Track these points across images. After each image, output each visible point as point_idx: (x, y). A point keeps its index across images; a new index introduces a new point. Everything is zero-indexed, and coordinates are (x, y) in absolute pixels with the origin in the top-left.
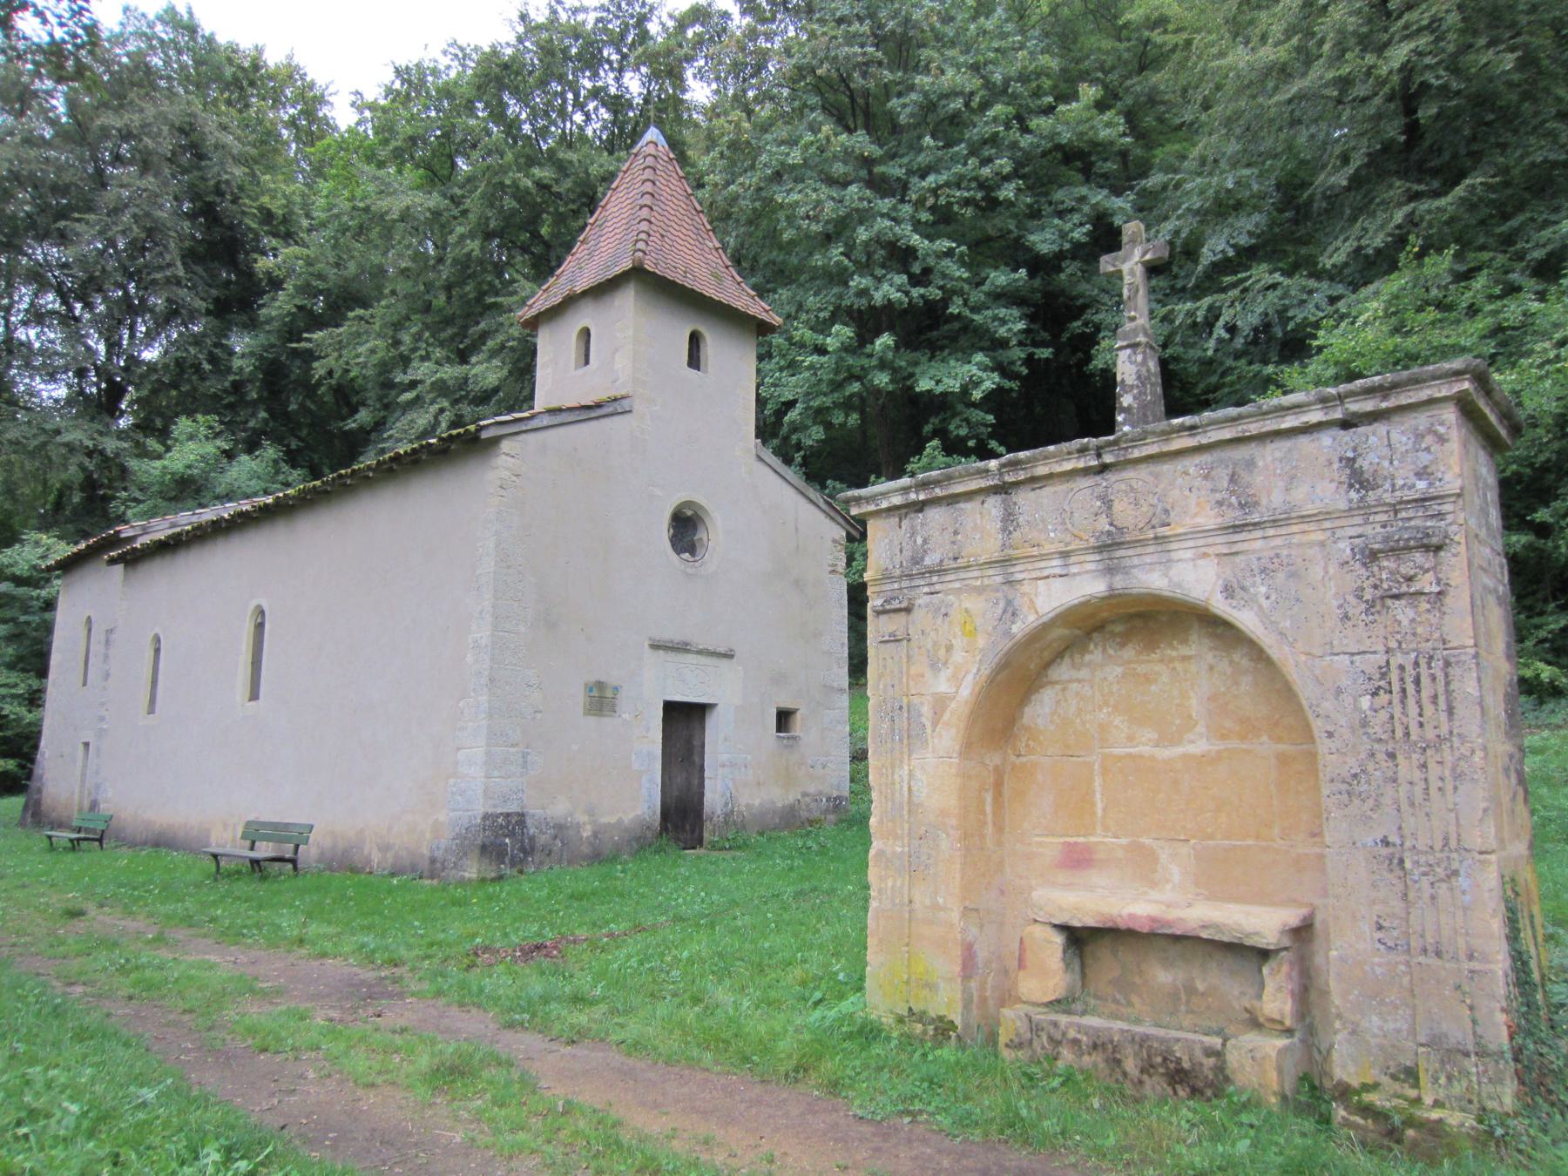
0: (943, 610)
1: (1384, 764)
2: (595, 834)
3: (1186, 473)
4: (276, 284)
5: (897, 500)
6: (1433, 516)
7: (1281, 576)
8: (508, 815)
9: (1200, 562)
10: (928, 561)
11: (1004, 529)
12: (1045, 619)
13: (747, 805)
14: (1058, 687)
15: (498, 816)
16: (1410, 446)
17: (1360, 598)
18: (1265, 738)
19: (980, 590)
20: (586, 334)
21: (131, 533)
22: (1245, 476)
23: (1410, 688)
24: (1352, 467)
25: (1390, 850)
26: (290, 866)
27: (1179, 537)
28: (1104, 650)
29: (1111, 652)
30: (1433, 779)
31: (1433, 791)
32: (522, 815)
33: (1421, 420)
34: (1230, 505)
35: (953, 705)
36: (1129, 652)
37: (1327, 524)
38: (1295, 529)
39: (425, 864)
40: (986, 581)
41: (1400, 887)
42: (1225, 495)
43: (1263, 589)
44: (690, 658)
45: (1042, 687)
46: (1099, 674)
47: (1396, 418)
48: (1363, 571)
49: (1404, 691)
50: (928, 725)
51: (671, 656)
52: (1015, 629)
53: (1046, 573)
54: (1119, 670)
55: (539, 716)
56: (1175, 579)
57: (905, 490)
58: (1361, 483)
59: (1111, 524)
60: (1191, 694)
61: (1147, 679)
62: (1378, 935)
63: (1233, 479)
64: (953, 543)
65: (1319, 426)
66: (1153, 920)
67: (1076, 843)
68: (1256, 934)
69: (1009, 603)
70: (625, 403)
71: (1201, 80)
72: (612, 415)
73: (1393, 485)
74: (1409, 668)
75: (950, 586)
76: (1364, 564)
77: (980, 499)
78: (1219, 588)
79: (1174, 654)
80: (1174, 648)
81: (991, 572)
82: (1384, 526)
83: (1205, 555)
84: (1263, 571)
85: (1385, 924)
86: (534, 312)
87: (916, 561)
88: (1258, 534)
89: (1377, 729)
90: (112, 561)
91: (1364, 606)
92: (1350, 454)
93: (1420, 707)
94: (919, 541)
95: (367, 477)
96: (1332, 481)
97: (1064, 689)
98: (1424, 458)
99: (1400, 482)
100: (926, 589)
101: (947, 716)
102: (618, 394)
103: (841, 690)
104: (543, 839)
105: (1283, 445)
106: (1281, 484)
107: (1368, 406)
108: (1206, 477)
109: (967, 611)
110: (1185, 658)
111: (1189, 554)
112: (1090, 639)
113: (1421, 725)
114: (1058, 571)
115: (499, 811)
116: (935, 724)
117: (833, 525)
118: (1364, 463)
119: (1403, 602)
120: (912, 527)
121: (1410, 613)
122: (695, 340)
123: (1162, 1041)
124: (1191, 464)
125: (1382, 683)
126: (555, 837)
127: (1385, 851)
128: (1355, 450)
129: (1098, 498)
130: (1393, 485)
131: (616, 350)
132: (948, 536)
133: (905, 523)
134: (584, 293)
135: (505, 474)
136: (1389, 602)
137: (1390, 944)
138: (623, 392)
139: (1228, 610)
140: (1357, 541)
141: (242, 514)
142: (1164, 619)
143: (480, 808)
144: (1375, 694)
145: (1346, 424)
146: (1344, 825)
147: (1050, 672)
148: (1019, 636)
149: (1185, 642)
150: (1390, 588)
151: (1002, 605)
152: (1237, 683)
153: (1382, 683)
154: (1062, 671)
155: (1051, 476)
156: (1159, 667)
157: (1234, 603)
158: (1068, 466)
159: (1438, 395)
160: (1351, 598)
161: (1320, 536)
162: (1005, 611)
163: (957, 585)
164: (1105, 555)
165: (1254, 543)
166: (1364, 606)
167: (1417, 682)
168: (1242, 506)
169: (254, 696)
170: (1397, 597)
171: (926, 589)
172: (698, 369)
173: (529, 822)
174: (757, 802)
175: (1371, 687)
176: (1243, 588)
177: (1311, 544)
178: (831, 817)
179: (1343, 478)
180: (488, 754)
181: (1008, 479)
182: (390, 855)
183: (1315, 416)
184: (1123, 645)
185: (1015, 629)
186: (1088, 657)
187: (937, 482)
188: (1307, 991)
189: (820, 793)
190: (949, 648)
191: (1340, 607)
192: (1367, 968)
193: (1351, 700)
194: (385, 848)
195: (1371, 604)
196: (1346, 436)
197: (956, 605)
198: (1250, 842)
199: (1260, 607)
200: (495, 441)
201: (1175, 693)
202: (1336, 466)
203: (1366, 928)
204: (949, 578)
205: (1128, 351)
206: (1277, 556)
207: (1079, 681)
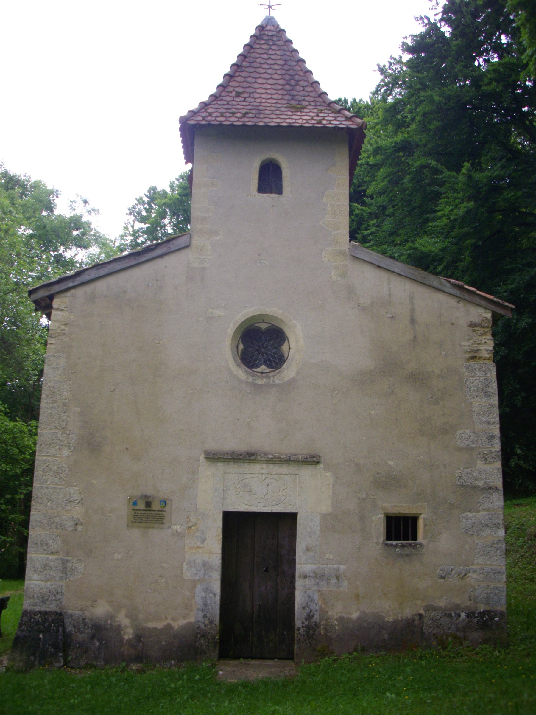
2: (138, 637)
4: (410, 128)
8: (46, 613)
13: (341, 619)
15: (36, 613)
44: (258, 468)
51: (233, 469)
71: (24, 325)
72: (166, 254)
103: (490, 489)
115: (37, 609)
117: (441, 297)
126: (93, 637)
173: (67, 621)
174: (355, 615)
178: (476, 635)
188: (257, 114)
189: (457, 607)
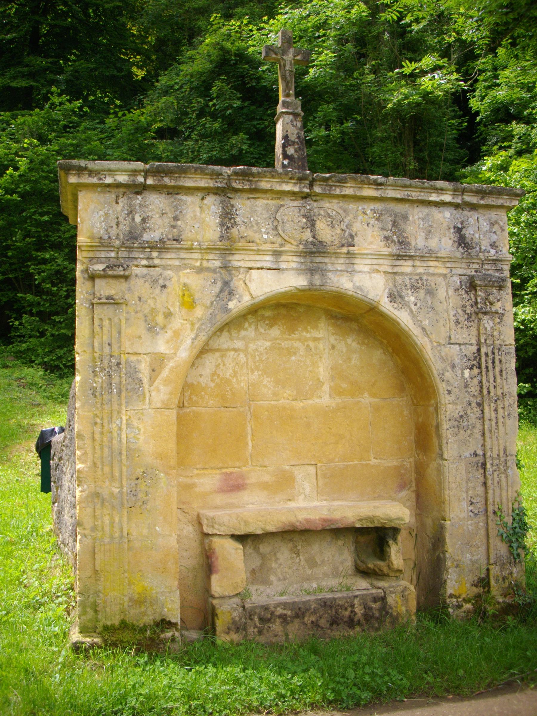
0: (161, 282)
1: (475, 409)
3: (365, 213)
5: (122, 178)
6: (498, 270)
7: (422, 293)
9: (374, 275)
10: (146, 237)
11: (222, 224)
12: (257, 300)
14: (217, 354)
16: (488, 228)
17: (465, 311)
18: (366, 395)
19: (200, 270)
22: (402, 225)
23: (490, 366)
24: (460, 233)
25: (477, 458)
27: (363, 256)
28: (256, 329)
29: (262, 330)
30: (500, 417)
31: (500, 424)
33: (493, 215)
34: (393, 241)
35: (172, 364)
36: (275, 332)
37: (448, 265)
38: (432, 264)
40: (205, 264)
41: (482, 479)
42: (389, 233)
43: (412, 299)
46: (252, 346)
47: (481, 211)
48: (465, 296)
49: (487, 367)
50: (145, 381)
52: (231, 305)
53: (259, 265)
56: (357, 284)
57: (135, 172)
58: (465, 244)
59: (314, 237)
60: (320, 364)
61: (291, 352)
62: (471, 508)
64: (173, 227)
65: (449, 204)
67: (231, 473)
68: (398, 519)
69: (226, 284)
73: (480, 249)
74: (490, 354)
75: (170, 262)
76: (467, 292)
77: (200, 195)
78: (386, 295)
79: (308, 335)
80: (307, 332)
81: (211, 256)
82: (476, 271)
83: (378, 271)
84: (413, 287)
85: (474, 501)
88: (410, 263)
89: (473, 389)
91: (466, 316)
92: (460, 226)
93: (495, 378)
94: (138, 219)
96: (450, 239)
98: (494, 237)
100: (145, 262)
101: (165, 373)
105: (426, 210)
106: (423, 234)
107: (474, 199)
108: (378, 219)
109: (185, 285)
110: (316, 339)
111: (366, 269)
112: (246, 319)
113: (495, 387)
114: (269, 265)
116: (152, 380)
118: (468, 232)
119: (488, 317)
121: (491, 323)
123: (304, 602)
124: (369, 207)
125: (475, 362)
127: (475, 459)
128: (462, 224)
129: (304, 216)
130: (480, 249)
132: (167, 220)
133: (122, 201)
136: (480, 315)
137: (476, 512)
139: (392, 309)
140: (463, 277)
142: (301, 310)
144: (471, 369)
146: (456, 446)
148: (234, 311)
149: (316, 327)
150: (482, 308)
151: (219, 284)
152: (350, 359)
153: (475, 362)
155: (271, 191)
156: (297, 344)
157: (396, 305)
158: (287, 187)
160: (460, 311)
161: (444, 271)
162: (221, 291)
163: (177, 263)
164: (308, 259)
165: (406, 267)
166: (466, 316)
167: (493, 362)
168: (400, 243)
170: (485, 313)
171: (145, 262)
175: (469, 364)
176: (401, 296)
177: (440, 275)
179: (456, 239)
184: (271, 326)
185: (231, 305)
186: (243, 333)
187: (169, 173)
191: (455, 315)
192: (465, 528)
193: (460, 372)
195: (470, 316)
196: (458, 214)
197: (175, 279)
198: (356, 462)
199: (411, 311)
201: (308, 362)
202: (452, 230)
203: (465, 504)
204: (169, 256)
205: (291, 117)
206: (421, 279)
207: (235, 350)
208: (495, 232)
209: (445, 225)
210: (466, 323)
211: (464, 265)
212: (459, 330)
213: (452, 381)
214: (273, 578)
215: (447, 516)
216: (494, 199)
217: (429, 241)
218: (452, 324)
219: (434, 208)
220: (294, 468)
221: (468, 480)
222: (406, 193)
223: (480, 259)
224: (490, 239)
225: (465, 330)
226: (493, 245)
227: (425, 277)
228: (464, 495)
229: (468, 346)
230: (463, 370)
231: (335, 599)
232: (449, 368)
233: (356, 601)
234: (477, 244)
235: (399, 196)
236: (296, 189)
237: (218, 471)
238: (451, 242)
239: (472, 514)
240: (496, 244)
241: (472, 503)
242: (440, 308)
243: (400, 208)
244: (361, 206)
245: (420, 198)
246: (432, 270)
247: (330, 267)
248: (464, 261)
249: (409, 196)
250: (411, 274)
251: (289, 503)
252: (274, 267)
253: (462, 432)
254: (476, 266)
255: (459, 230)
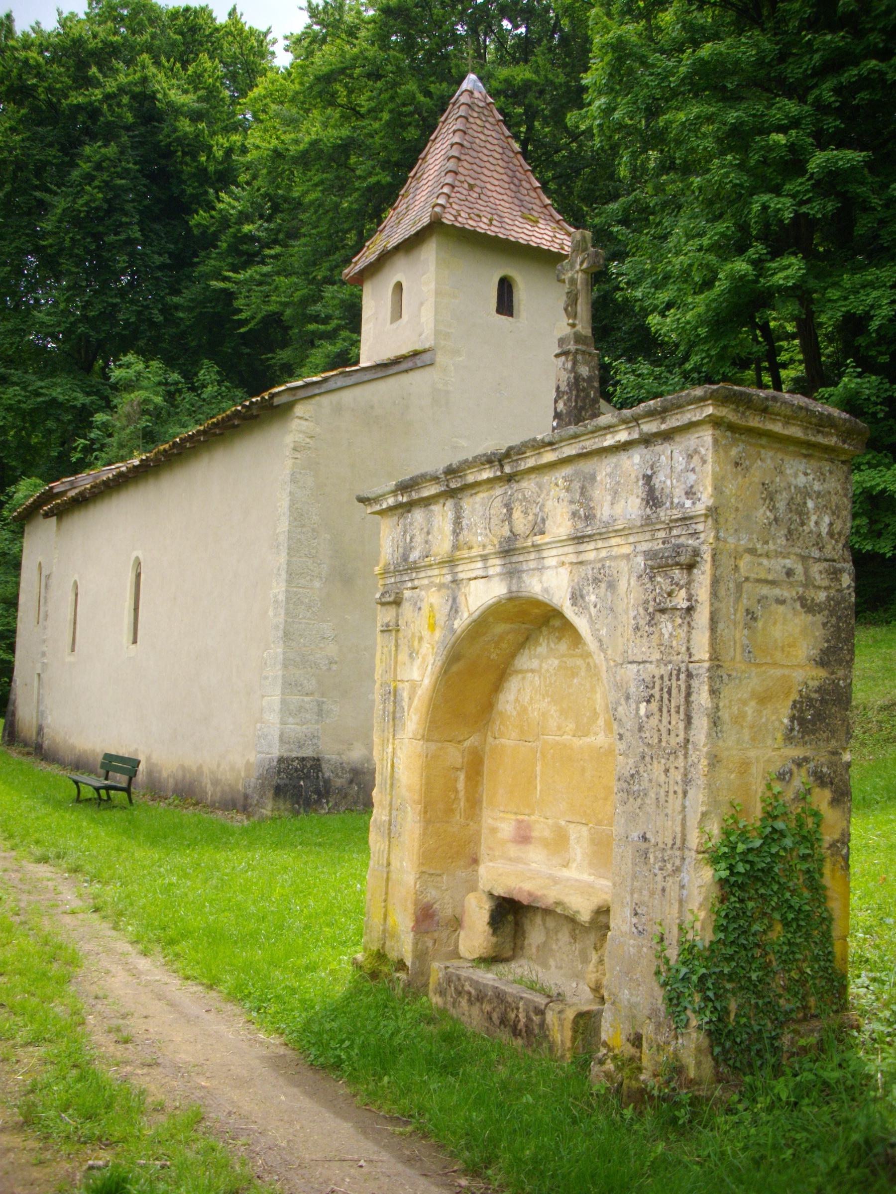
8: (303, 759)
14: (520, 676)
20: (399, 286)
21: (61, 489)
26: (124, 795)
29: (552, 645)
32: (318, 760)
37: (631, 539)
38: (614, 541)
39: (241, 801)
43: (593, 598)
45: (510, 675)
49: (662, 698)
53: (473, 575)
54: (556, 662)
55: (334, 667)
60: (598, 690)
62: (634, 920)
63: (583, 488)
65: (625, 446)
66: (530, 894)
70: (426, 357)
73: (672, 503)
78: (569, 596)
83: (563, 564)
85: (639, 911)
86: (357, 269)
87: (405, 558)
88: (592, 546)
90: (47, 515)
92: (649, 472)
95: (215, 435)
97: (524, 678)
99: (676, 500)
100: (409, 585)
102: (418, 347)
104: (338, 782)
114: (480, 573)
115: (294, 755)
118: (661, 479)
119: (666, 616)
120: (405, 526)
122: (505, 289)
124: (560, 475)
130: (672, 503)
131: (422, 304)
134: (397, 248)
135: (299, 437)
137: (640, 928)
138: (427, 346)
141: (121, 475)
143: (276, 752)
144: (648, 702)
145: (647, 440)
146: (623, 821)
147: (516, 662)
154: (524, 661)
159: (694, 419)
160: (641, 610)
161: (626, 550)
169: (135, 641)
171: (409, 585)
172: (511, 314)
179: (644, 496)
180: (283, 702)
181: (453, 485)
182: (219, 789)
183: (623, 436)
184: (560, 639)
186: (539, 649)
190: (421, 639)
191: (635, 618)
194: (216, 782)
200: (289, 407)
202: (641, 483)
203: (628, 912)
206: (603, 566)
208: (693, 470)
209: (633, 476)
210: (647, 628)
211: (648, 536)
212: (638, 640)
213: (624, 720)
214: (552, 962)
215: (612, 925)
216: (678, 416)
217: (615, 506)
218: (630, 631)
219: (622, 453)
220: (572, 826)
221: (634, 877)
222: (581, 444)
223: (664, 522)
224: (685, 483)
225: (644, 640)
226: (690, 493)
227: (608, 563)
228: (628, 899)
229: (648, 665)
230: (638, 703)
231: (505, 993)
232: (623, 701)
233: (521, 1004)
234: (667, 497)
235: (574, 452)
236: (491, 475)
237: (513, 817)
238: (639, 500)
239: (634, 929)
240: (694, 490)
241: (636, 914)
242: (620, 607)
243: (586, 466)
244: (547, 478)
245: (594, 447)
246: (616, 551)
247: (525, 567)
248: (646, 529)
249: (584, 448)
250: (594, 561)
251: (564, 869)
252: (484, 574)
253: (631, 800)
254: (662, 534)
255: (648, 479)
